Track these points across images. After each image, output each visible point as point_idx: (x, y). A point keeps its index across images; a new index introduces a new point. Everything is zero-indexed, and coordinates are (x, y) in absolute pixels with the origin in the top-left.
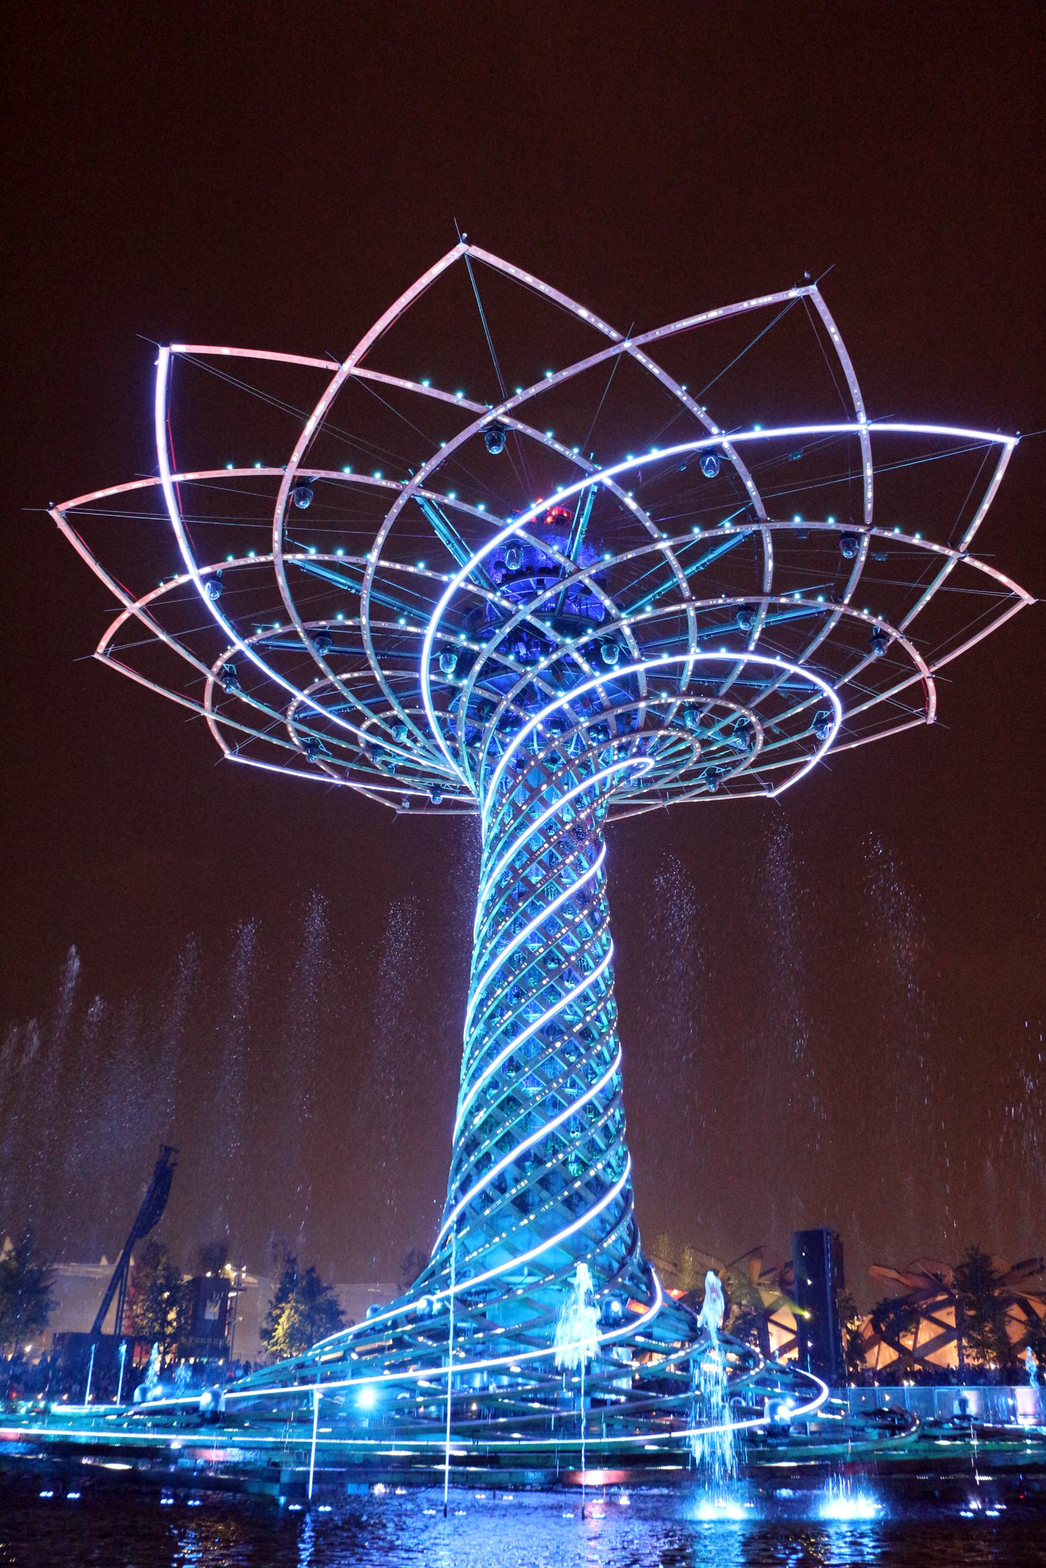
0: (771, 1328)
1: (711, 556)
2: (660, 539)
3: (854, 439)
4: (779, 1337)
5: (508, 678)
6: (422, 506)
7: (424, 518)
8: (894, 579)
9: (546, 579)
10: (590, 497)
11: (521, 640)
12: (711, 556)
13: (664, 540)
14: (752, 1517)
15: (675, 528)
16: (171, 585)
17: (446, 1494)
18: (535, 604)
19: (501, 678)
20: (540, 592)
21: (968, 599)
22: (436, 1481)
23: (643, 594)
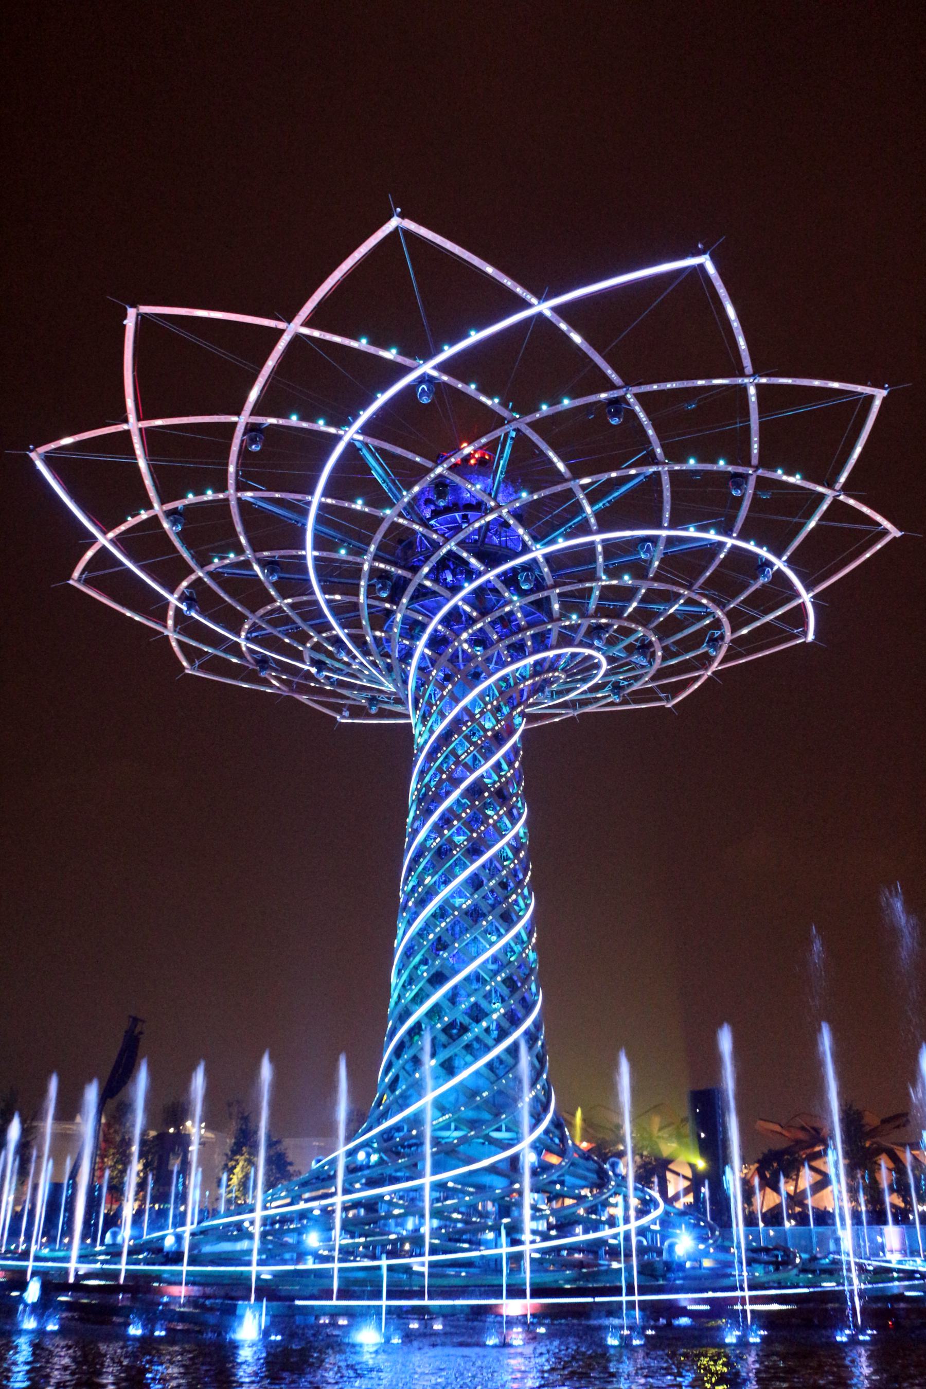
1: (616, 494)
6: (360, 450)
7: (362, 459)
11: (448, 568)
12: (616, 494)
21: (844, 533)
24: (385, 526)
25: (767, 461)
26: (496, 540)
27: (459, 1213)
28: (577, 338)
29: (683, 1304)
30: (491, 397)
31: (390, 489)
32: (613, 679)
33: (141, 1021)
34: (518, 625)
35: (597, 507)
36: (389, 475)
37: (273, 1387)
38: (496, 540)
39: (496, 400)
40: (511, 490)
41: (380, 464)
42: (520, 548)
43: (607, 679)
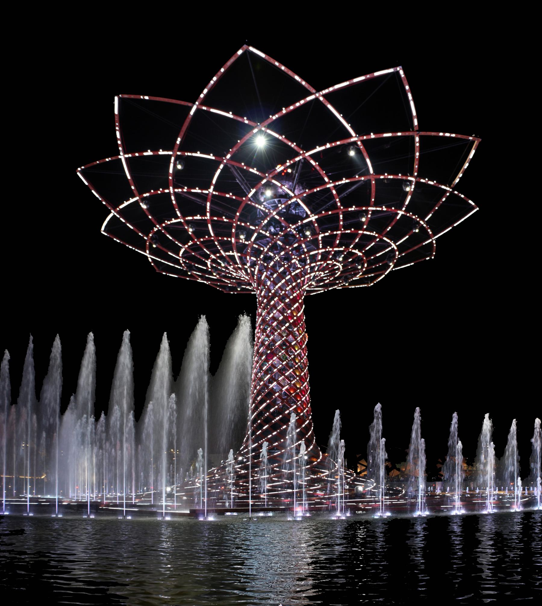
0: (358, 465)
1: (350, 190)
2: (329, 183)
3: (30, 505)
4: (361, 468)
5: (267, 240)
6: (230, 168)
7: (231, 173)
8: (329, 242)
9: (282, 199)
10: (300, 164)
11: (272, 225)
12: (350, 190)
13: (331, 183)
14: (253, 161)
15: (334, 179)
16: (129, 202)
17: (250, 515)
18: (294, 455)
19: (264, 241)
20: (279, 205)
21: (456, 207)
22: (247, 511)
23: (322, 206)
24: (243, 205)
25: (420, 176)
26: (294, 212)
27: (111, 451)
28: (297, 78)
29: (86, 439)
30: (352, 207)
31: (245, 188)
32: (345, 275)
33: (307, 511)
34: (304, 251)
35: (341, 196)
36: (244, 181)
37: (221, 603)
38: (294, 212)
39: (354, 207)
40: (301, 188)
41: (240, 176)
42: (305, 216)
43: (342, 275)
